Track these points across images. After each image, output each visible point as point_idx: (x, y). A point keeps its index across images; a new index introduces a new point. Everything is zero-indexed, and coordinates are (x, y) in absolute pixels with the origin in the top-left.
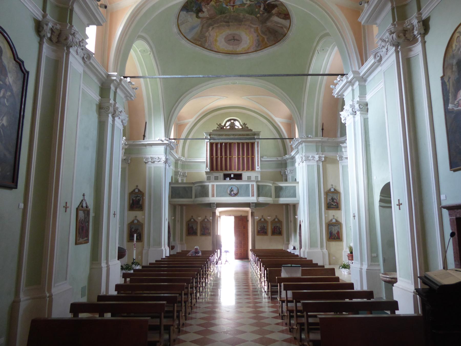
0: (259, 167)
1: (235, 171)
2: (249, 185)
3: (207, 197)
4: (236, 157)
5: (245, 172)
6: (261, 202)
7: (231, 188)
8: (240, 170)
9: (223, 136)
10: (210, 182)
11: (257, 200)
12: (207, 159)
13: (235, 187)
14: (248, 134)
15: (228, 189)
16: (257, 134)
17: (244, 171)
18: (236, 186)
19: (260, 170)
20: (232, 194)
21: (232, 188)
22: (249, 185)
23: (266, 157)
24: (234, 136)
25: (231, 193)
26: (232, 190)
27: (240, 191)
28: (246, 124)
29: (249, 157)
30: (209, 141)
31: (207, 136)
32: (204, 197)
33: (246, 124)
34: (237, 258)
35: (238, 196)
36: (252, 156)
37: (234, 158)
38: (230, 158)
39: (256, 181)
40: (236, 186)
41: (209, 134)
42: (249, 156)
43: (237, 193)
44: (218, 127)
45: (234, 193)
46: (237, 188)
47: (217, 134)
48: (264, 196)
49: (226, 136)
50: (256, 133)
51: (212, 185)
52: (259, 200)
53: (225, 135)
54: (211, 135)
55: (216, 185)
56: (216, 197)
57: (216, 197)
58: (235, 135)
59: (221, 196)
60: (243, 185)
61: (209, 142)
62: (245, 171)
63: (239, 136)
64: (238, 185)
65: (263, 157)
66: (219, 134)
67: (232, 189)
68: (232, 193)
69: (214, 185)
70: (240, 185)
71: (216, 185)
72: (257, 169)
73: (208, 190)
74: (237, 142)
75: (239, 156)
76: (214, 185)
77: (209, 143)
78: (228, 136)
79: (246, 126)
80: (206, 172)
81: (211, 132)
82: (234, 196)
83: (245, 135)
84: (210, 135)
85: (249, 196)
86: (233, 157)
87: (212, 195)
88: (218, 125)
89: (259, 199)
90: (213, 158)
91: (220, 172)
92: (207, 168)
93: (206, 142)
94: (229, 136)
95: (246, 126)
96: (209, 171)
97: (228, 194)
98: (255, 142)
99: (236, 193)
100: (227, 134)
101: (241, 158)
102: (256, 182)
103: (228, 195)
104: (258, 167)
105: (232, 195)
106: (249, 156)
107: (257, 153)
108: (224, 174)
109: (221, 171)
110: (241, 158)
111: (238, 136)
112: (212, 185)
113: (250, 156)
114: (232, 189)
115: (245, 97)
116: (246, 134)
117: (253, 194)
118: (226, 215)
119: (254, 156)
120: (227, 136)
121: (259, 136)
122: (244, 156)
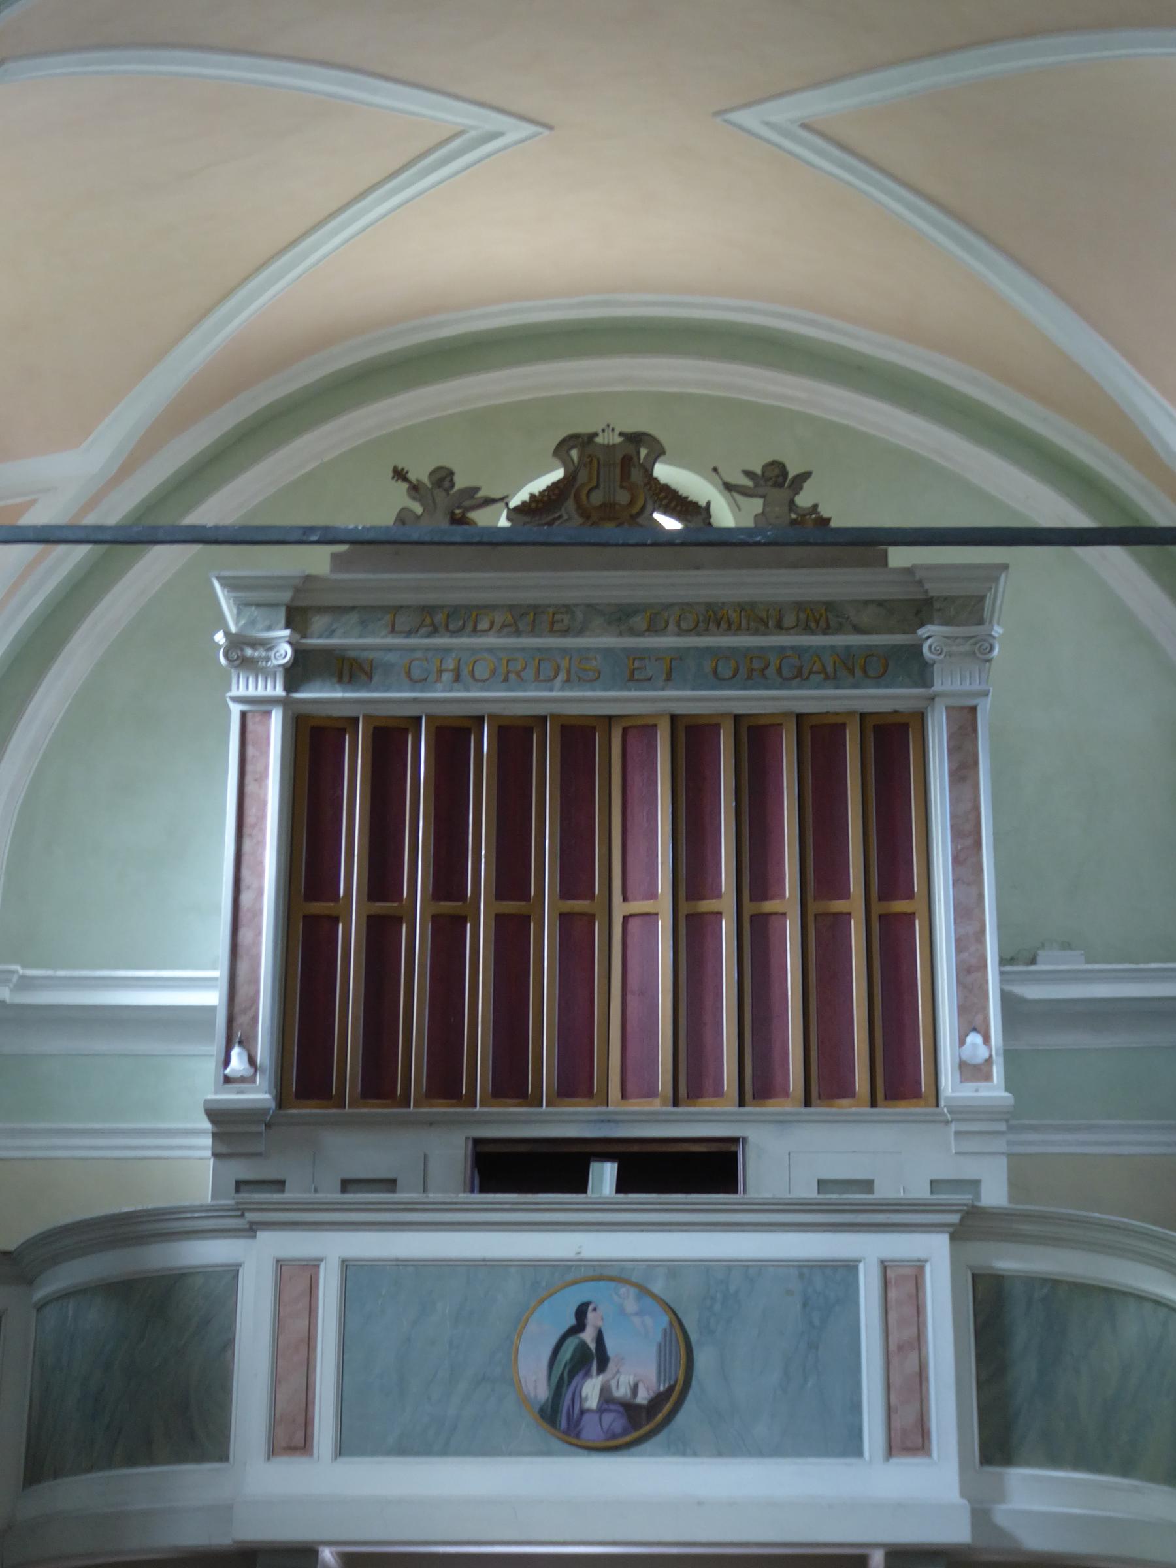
0: (987, 1039)
1: (636, 1106)
2: (849, 1268)
3: (201, 1458)
4: (652, 916)
5: (782, 1122)
6: (1035, 1541)
7: (572, 1321)
8: (718, 1093)
9: (475, 631)
10: (251, 1230)
11: (980, 1516)
12: (245, 935)
13: (631, 1306)
14: (829, 606)
15: (519, 1323)
16: (949, 600)
17: (772, 1108)
18: (644, 1291)
19: (995, 1090)
20: (592, 1402)
21: (581, 1313)
22: (849, 1268)
23: (1074, 962)
24: (633, 632)
25: (577, 1396)
26: (583, 1345)
27: (704, 1359)
28: (792, 472)
29: (843, 918)
30: (279, 691)
31: (252, 623)
32: (152, 1461)
33: (792, 472)
34: (254, 1237)
35: (683, 1448)
36: (885, 896)
37: (633, 924)
38: (565, 920)
39: (955, 1218)
40: (644, 1291)
41: (286, 596)
42: (839, 906)
43: (659, 1400)
44: (418, 508)
45: (621, 1391)
46: (664, 1320)
47: (397, 609)
48: (1083, 1461)
49: (518, 633)
50: (934, 589)
51: (280, 1264)
52: (1002, 1515)
53: (499, 618)
54: (319, 622)
55: (346, 1265)
56: (341, 1450)
57: (341, 1450)
58: (640, 622)
59: (403, 1449)
60: (752, 1270)
61: (284, 702)
62: (789, 1106)
63: (707, 632)
64: (674, 1268)
65: (1033, 961)
66: (428, 610)
67: (579, 1326)
68: (591, 1390)
69: (311, 1268)
70: (705, 1268)
71: (346, 1265)
72: (973, 1071)
73: (228, 1344)
74: (674, 718)
75: (707, 905)
76: (311, 1268)
77: (276, 721)
78: (552, 631)
79: (804, 500)
80: (216, 1115)
81: (308, 578)
82: (612, 1446)
83: (789, 620)
84: (296, 617)
85: (851, 1446)
86: (620, 909)
87: (275, 1422)
88: (415, 489)
89: (1001, 1497)
90: (335, 920)
91: (431, 1123)
92: (236, 1052)
93: (236, 709)
94: (566, 632)
95: (804, 500)
96: (260, 1094)
97: (524, 1400)
98: (921, 717)
99: (643, 1398)
100: (537, 610)
101: (727, 928)
102: (957, 1235)
103: (530, 1428)
104: (974, 1039)
105: (591, 1430)
106: (839, 906)
107: (957, 860)
108: (477, 1142)
109: (442, 1109)
110: (727, 928)
111: (681, 632)
112: (280, 1264)
113: (854, 904)
114: (588, 1336)
115: (785, 111)
116: (799, 606)
117: (906, 1417)
118: (204, 527)
119: (910, 895)
120: (533, 631)
121: (981, 622)
122: (769, 906)
